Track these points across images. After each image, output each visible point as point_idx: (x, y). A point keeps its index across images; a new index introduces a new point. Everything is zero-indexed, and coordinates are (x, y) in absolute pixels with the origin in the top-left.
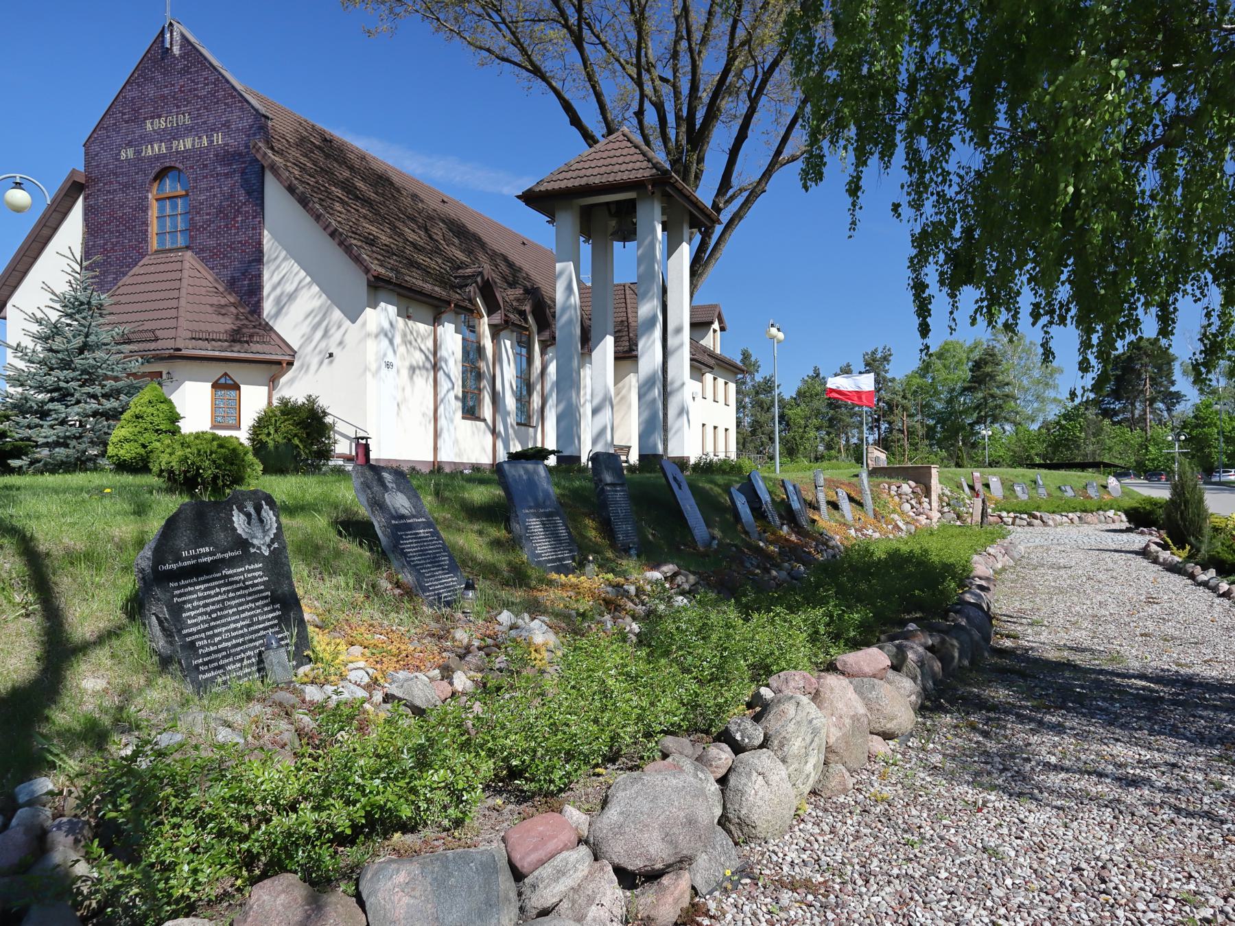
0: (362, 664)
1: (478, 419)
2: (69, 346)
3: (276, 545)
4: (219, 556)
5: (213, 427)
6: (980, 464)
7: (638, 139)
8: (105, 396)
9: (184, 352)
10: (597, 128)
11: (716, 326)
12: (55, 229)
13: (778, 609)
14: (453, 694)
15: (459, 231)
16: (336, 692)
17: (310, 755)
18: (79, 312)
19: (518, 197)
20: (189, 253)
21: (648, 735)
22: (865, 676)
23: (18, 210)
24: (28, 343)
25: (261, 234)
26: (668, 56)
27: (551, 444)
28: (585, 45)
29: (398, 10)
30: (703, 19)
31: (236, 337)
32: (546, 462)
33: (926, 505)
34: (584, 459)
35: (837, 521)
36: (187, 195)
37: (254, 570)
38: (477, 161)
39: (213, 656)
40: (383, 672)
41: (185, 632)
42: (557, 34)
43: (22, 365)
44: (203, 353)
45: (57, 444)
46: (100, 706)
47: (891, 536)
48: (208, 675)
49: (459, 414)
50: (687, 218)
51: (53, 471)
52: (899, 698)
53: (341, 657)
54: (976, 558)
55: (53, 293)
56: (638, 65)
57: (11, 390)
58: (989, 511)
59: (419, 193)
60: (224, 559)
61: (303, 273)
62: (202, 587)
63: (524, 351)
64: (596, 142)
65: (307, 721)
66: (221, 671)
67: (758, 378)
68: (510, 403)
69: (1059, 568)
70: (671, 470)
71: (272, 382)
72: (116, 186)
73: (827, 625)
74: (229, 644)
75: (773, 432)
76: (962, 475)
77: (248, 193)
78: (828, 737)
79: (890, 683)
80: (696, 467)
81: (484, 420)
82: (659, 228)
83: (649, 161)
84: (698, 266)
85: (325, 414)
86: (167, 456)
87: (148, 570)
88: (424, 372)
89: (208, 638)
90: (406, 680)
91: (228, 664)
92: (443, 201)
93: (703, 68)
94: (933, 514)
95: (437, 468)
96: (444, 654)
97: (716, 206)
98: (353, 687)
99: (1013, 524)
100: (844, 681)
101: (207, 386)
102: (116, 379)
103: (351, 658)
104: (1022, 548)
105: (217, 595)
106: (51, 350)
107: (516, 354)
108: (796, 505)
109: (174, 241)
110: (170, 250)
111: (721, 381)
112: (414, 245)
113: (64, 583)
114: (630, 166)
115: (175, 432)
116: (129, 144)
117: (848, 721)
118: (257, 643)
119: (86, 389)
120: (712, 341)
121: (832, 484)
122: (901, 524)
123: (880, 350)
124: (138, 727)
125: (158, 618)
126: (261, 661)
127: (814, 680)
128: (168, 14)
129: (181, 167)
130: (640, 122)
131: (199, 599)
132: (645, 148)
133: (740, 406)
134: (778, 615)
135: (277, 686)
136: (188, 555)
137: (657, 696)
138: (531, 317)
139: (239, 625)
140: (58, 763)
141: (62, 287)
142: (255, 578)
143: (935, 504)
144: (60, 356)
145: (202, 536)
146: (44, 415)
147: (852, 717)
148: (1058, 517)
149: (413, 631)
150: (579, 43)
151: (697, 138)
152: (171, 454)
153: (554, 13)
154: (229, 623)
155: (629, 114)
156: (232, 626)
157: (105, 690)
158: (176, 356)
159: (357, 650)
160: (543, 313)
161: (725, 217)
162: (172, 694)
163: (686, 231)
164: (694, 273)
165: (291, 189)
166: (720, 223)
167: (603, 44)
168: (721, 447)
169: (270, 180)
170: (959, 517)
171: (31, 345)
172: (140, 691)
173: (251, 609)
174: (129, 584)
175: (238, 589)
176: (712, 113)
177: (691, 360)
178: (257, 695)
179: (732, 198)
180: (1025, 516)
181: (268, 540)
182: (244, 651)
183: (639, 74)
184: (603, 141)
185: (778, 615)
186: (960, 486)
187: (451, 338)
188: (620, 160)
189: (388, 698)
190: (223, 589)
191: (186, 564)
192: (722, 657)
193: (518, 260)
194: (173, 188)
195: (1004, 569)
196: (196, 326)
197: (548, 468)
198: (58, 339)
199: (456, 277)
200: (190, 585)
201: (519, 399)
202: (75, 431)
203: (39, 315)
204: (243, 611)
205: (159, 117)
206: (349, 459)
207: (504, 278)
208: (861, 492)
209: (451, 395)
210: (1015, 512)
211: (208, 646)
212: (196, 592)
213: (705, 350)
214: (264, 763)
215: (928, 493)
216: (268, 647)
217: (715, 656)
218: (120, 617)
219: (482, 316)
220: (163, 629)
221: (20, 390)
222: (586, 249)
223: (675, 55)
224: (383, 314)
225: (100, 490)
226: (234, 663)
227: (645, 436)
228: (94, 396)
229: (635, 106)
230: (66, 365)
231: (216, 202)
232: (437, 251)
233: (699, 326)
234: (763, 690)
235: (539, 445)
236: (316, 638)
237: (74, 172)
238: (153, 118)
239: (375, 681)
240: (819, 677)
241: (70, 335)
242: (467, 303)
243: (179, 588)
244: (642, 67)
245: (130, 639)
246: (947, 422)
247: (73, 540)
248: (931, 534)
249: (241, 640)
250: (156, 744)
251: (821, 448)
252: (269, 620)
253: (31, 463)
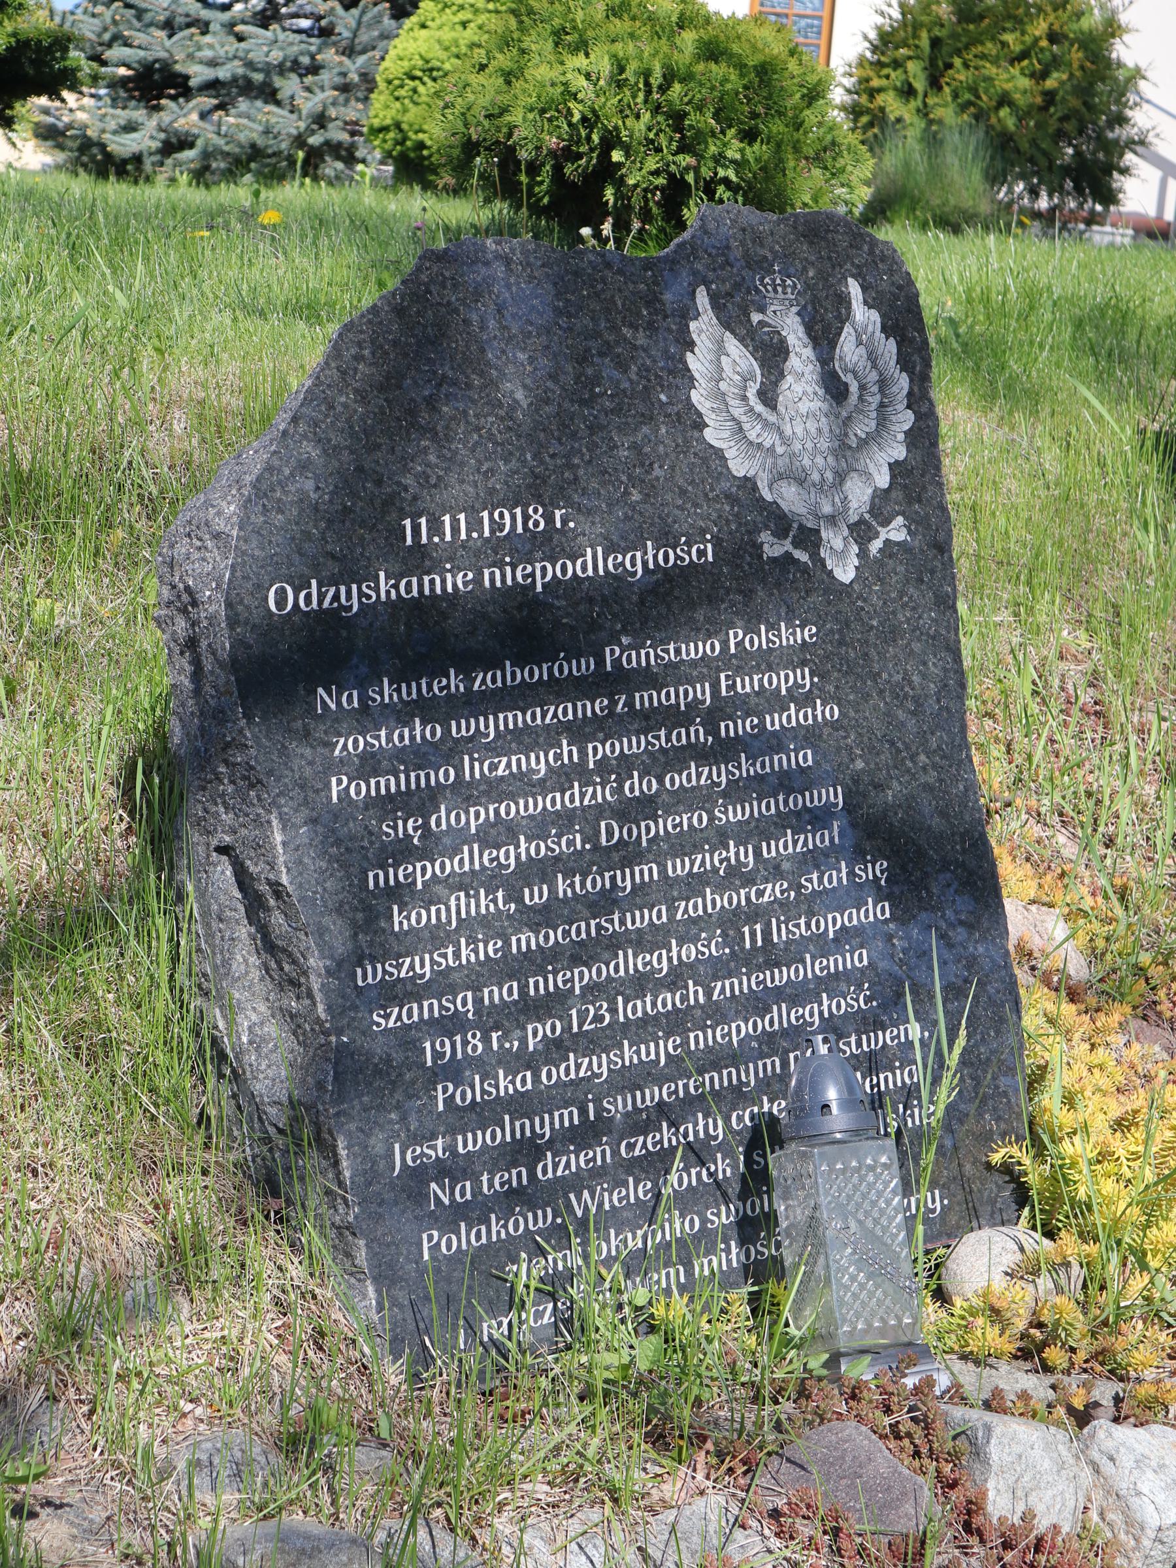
3: (896, 531)
37: (767, 661)
66: (543, 1219)
136: (471, 537)
139: (660, 962)
152: (509, 77)
173: (736, 876)
181: (858, 496)
190: (599, 750)
204: (694, 884)
249: (662, 1049)
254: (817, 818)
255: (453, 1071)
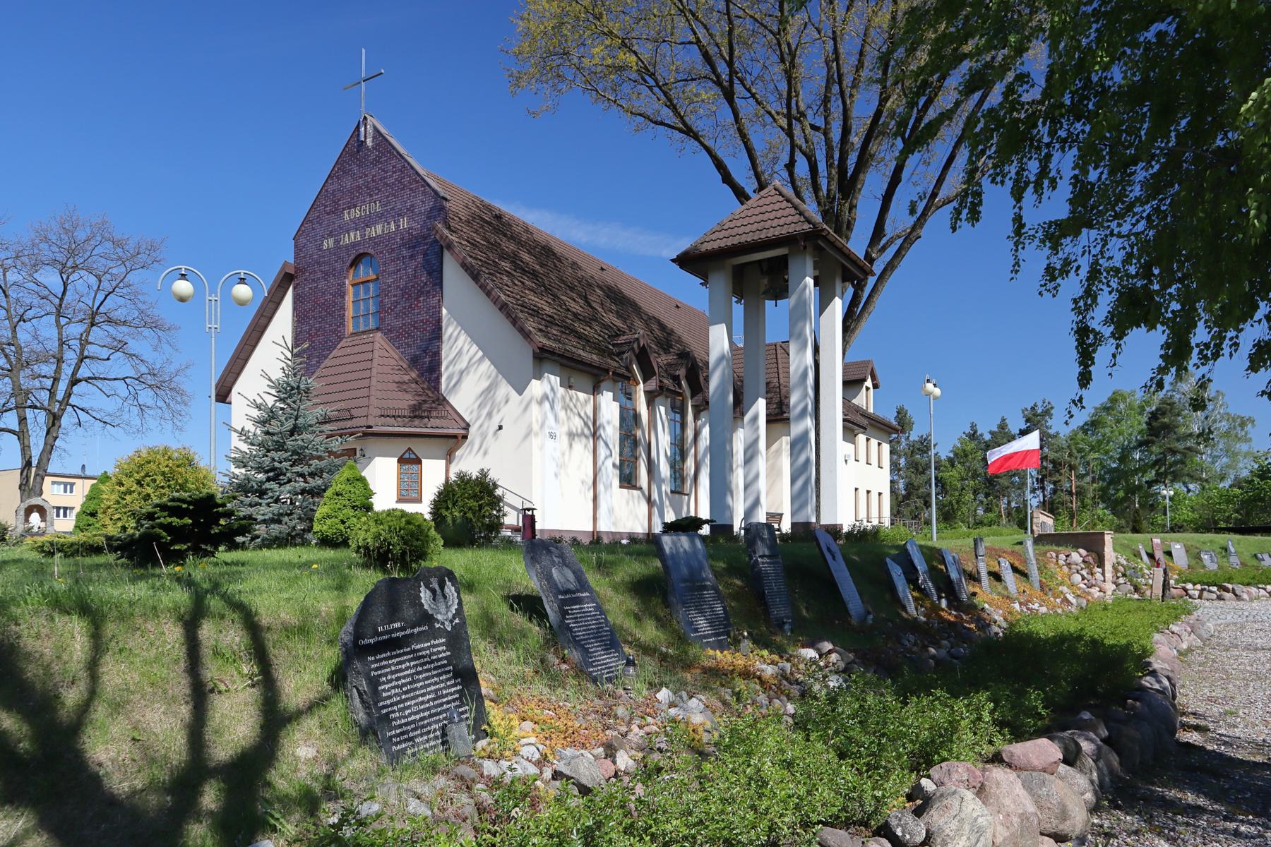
0: (533, 740)
1: (634, 487)
2: (283, 429)
3: (457, 621)
4: (409, 631)
5: (399, 501)
6: (1163, 529)
7: (789, 192)
8: (312, 475)
9: (375, 429)
10: (749, 185)
11: (869, 383)
12: (271, 318)
13: (938, 693)
14: (616, 775)
15: (617, 298)
16: (511, 769)
17: (489, 831)
18: (290, 396)
19: (673, 261)
20: (379, 334)
21: (806, 825)
22: (1034, 770)
23: (242, 303)
24: (250, 427)
25: (440, 312)
26: (819, 103)
27: (704, 514)
28: (737, 100)
29: (560, 86)
30: (854, 60)
31: (417, 413)
32: (700, 532)
33: (1099, 576)
34: (736, 529)
35: (999, 594)
36: (377, 279)
37: (438, 645)
38: (632, 227)
39: (404, 729)
40: (552, 748)
41: (380, 704)
42: (709, 93)
43: (244, 447)
44: (391, 429)
45: (273, 521)
46: (311, 773)
47: (1060, 611)
48: (400, 747)
49: (616, 482)
50: (839, 272)
51: (269, 547)
52: (1074, 792)
53: (516, 732)
54: (1157, 636)
55: (270, 380)
56: (789, 116)
57: (237, 471)
58: (1172, 582)
59: (579, 262)
60: (413, 634)
61: (475, 348)
62: (395, 661)
63: (678, 417)
64: (748, 198)
65: (486, 798)
67: (914, 436)
68: (665, 470)
69: (1256, 650)
70: (825, 540)
71: (449, 457)
72: (319, 275)
73: (992, 712)
74: (417, 717)
75: (929, 495)
76: (1140, 541)
77: (430, 274)
78: (994, 836)
79: (1062, 778)
80: (850, 534)
81: (640, 489)
82: (810, 281)
83: (801, 214)
84: (850, 321)
85: (495, 486)
86: (363, 533)
87: (350, 645)
88: (584, 440)
89: (399, 710)
90: (573, 758)
91: (416, 737)
92: (602, 269)
93: (854, 113)
94: (1107, 586)
95: (596, 540)
96: (607, 732)
97: (868, 256)
98: (526, 763)
99: (1200, 597)
100: (1011, 775)
101: (393, 462)
102: (320, 458)
103: (523, 734)
104: (1211, 626)
105: (407, 669)
106: (267, 433)
107: (670, 421)
108: (954, 575)
109: (366, 324)
110: (363, 333)
111: (874, 442)
112: (575, 315)
113: (279, 656)
114: (782, 221)
115: (369, 508)
116: (330, 235)
117: (1016, 820)
118: (441, 717)
119: (297, 469)
120: (865, 399)
121: (995, 554)
122: (1070, 597)
123: (1039, 404)
124: (343, 796)
125: (358, 691)
126: (444, 735)
127: (978, 773)
128: (363, 109)
129: (372, 252)
130: (791, 174)
131: (392, 673)
132: (797, 201)
133: (895, 467)
134: (938, 698)
135: (459, 761)
137: (815, 785)
138: (682, 380)
139: (425, 699)
140: (279, 827)
141: (277, 374)
142: (440, 652)
143: (1109, 575)
144: (275, 438)
145: (393, 612)
146: (262, 493)
147: (1021, 816)
148: (1253, 590)
149: (578, 707)
150: (729, 96)
151: (848, 186)
153: (706, 70)
154: (417, 696)
155: (780, 166)
156: (420, 699)
157: (315, 759)
158: (369, 434)
159: (528, 725)
160: (695, 373)
161: (878, 268)
162: (370, 764)
163: (839, 286)
164: (846, 329)
165: (464, 266)
166: (873, 274)
167: (753, 96)
168: (874, 513)
169: (447, 257)
170: (1137, 589)
171: (252, 429)
172: (344, 760)
173: (436, 683)
174: (332, 655)
175: (425, 664)
176: (864, 160)
177: (844, 420)
178: (442, 768)
179: (884, 249)
180: (1215, 589)
181: (450, 615)
182: (429, 724)
183: (790, 124)
184: (754, 197)
185: (938, 698)
186: (1137, 555)
187: (609, 406)
188: (772, 215)
189: (557, 775)
191: (381, 638)
192: (879, 744)
193: (670, 322)
194: (366, 273)
195: (1190, 650)
196: (385, 404)
197: (703, 538)
198: (274, 422)
199: (614, 345)
200: (386, 659)
201: (673, 467)
202: (285, 509)
203: (259, 401)
204: (422, 687)
205: (355, 206)
206: (516, 530)
207: (659, 343)
208: (1025, 561)
209: (609, 463)
210: (1202, 583)
211: (400, 718)
212: (389, 666)
213: (858, 410)
214: (449, 836)
215: (1101, 562)
216: (451, 721)
217: (872, 743)
218: (326, 687)
219: (638, 383)
220: (363, 702)
221: (243, 471)
222: (738, 310)
223: (826, 100)
224: (547, 384)
225: (307, 565)
226: (421, 735)
227: (798, 499)
228: (302, 475)
229: (785, 158)
230: (280, 447)
231: (402, 284)
232: (593, 319)
233: (852, 384)
234: (924, 782)
235: (692, 514)
236: (492, 713)
237: (286, 264)
238: (349, 208)
239: (545, 757)
240: (984, 770)
241: (283, 419)
242: (623, 371)
243: (376, 661)
244: (793, 116)
245: (336, 707)
246: (1123, 480)
247: (289, 616)
248: (1105, 609)
250: (358, 813)
251: (980, 512)
252: (452, 694)
253: (253, 539)
254: (448, 672)
255: (395, 719)
